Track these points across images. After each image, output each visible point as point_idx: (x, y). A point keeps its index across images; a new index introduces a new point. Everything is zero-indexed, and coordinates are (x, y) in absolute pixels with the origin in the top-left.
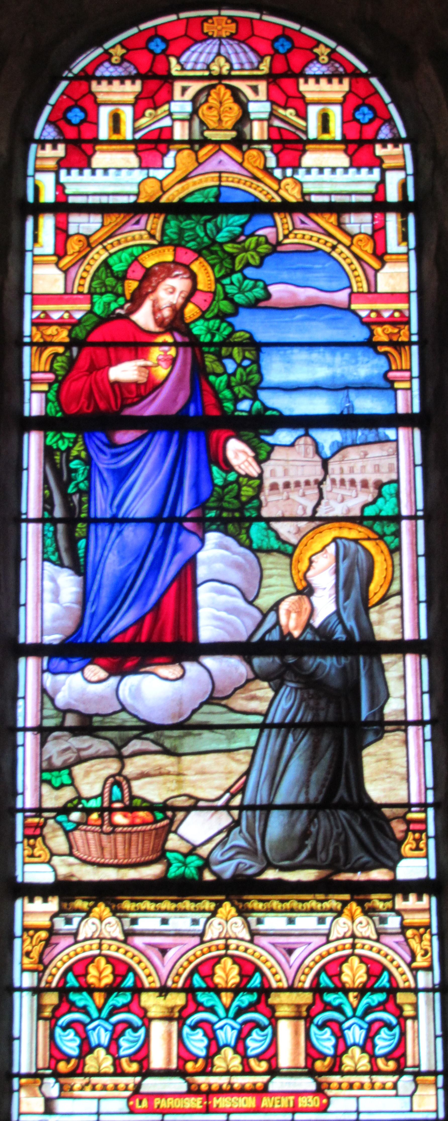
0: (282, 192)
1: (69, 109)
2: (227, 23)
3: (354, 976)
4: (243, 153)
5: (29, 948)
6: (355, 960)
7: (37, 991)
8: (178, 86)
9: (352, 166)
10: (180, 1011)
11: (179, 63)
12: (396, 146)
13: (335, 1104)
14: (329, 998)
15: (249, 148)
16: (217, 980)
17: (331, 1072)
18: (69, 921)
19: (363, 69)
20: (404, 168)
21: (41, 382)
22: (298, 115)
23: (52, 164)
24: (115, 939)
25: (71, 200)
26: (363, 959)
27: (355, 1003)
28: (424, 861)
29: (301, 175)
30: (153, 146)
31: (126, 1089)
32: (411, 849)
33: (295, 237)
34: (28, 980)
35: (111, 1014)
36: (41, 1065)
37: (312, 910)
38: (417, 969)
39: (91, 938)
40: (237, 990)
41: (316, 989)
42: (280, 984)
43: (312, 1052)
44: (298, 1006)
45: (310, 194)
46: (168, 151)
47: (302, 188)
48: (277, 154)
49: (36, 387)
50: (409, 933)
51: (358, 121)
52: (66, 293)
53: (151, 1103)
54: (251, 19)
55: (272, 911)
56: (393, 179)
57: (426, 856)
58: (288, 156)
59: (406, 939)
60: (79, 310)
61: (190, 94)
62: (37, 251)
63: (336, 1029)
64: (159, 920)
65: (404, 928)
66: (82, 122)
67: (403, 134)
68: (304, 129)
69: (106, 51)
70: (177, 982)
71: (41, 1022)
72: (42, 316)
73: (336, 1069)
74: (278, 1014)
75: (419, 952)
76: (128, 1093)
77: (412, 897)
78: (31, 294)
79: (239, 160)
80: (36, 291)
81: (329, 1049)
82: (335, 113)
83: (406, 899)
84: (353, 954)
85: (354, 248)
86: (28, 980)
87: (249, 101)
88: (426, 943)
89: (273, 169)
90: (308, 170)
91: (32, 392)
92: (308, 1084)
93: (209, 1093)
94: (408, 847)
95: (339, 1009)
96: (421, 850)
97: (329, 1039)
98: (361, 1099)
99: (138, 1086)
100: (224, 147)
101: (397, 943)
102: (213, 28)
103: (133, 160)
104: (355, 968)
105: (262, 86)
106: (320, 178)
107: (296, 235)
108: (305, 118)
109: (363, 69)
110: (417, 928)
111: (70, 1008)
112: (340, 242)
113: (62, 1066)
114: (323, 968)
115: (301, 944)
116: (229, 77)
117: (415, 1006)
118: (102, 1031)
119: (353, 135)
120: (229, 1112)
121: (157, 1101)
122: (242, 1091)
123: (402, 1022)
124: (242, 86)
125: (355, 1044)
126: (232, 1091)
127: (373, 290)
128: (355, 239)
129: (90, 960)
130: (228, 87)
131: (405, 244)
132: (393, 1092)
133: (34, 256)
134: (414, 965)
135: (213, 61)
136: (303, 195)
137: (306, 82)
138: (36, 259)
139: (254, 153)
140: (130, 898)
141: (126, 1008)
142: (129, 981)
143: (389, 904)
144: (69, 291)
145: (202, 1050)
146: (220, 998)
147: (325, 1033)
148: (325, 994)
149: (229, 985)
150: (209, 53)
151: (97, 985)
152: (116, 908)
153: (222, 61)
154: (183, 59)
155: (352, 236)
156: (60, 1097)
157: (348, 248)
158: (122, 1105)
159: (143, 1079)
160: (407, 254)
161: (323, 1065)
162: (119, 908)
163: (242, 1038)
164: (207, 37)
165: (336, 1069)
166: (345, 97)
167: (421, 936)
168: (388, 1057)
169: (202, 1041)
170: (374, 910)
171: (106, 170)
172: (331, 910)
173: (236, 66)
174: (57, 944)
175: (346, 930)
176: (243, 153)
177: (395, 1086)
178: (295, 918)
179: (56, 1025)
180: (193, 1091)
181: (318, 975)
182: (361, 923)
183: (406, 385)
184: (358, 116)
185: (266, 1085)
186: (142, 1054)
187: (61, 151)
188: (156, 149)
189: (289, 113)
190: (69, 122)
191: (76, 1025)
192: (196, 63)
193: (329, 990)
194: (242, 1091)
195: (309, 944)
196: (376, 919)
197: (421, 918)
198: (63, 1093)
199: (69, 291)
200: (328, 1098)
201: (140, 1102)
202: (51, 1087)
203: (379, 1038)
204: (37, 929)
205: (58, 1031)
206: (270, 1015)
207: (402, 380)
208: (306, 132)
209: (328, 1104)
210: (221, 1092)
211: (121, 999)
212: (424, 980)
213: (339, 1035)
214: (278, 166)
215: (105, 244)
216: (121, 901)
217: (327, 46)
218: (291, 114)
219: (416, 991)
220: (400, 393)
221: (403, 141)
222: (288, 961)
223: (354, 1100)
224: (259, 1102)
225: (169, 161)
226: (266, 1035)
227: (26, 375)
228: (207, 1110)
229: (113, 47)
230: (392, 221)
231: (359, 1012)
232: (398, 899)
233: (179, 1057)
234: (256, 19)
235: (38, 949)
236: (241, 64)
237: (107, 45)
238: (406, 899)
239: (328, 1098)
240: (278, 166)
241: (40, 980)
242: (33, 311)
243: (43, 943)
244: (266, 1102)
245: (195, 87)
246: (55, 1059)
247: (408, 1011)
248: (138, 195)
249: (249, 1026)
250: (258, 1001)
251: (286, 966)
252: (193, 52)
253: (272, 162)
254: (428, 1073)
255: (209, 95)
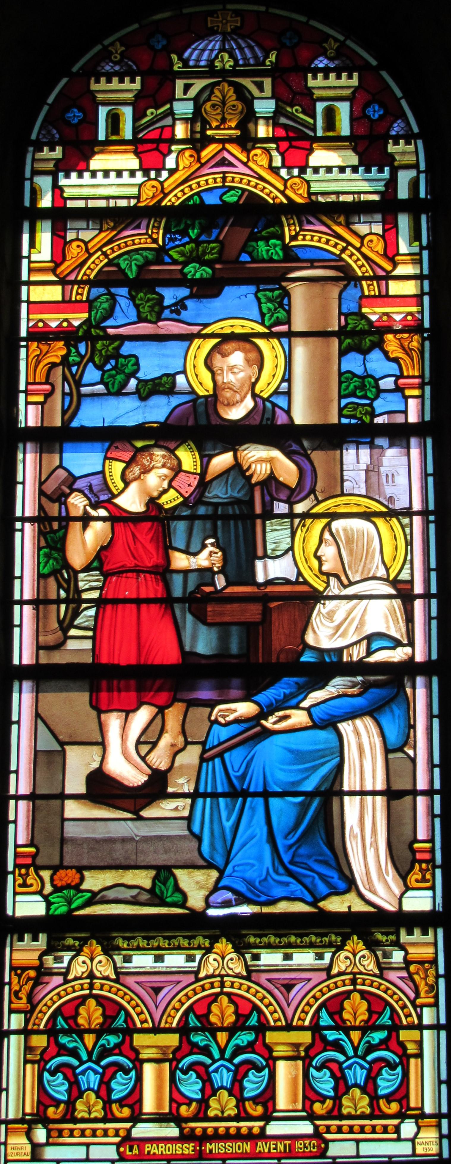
0: (289, 192)
1: (67, 110)
2: (231, 17)
3: (355, 1014)
4: (248, 152)
5: (17, 988)
6: (357, 996)
7: (26, 1032)
8: (180, 84)
9: (361, 164)
10: (174, 1052)
11: (180, 58)
12: (408, 143)
13: (334, 1150)
14: (64, 1040)
15: (254, 148)
16: (213, 1019)
17: (329, 1116)
18: (58, 960)
19: (374, 63)
20: (416, 166)
21: (36, 393)
22: (304, 112)
23: (50, 166)
24: (107, 978)
25: (70, 204)
26: (364, 995)
27: (223, 1044)
28: (430, 893)
29: (309, 175)
30: (154, 146)
31: (117, 1135)
32: (417, 881)
33: (304, 239)
34: (16, 1021)
35: (235, 1055)
36: (28, 1110)
37: (179, 948)
38: (422, 1006)
39: (212, 976)
40: (366, 1029)
41: (183, 1030)
42: (145, 1025)
43: (311, 1095)
44: (296, 1046)
45: (316, 194)
46: (170, 152)
47: (309, 187)
48: (282, 154)
49: (31, 399)
50: (412, 968)
51: (369, 117)
52: (63, 301)
53: (141, 1149)
54: (258, 13)
55: (138, 948)
56: (404, 178)
57: (433, 888)
58: (295, 156)
59: (410, 975)
60: (375, 313)
61: (193, 93)
62: (34, 258)
63: (70, 1074)
64: (183, 957)
65: (407, 962)
66: (81, 122)
67: (416, 130)
68: (312, 127)
69: (105, 48)
70: (304, 1020)
71: (29, 1066)
72: (65, 324)
73: (70, 1117)
74: (141, 1056)
75: (423, 988)
76: (117, 1140)
77: (417, 931)
78: (28, 302)
79: (245, 160)
80: (32, 299)
81: (328, 1091)
82: (343, 110)
83: (410, 933)
84: (222, 993)
85: (364, 250)
86: (16, 1021)
87: (253, 98)
88: (431, 980)
89: (278, 168)
90: (316, 170)
91: (27, 403)
92: (306, 1128)
93: (204, 1138)
94: (415, 877)
95: (206, 1051)
96: (427, 881)
97: (63, 1084)
98: (92, 1147)
99: (129, 1131)
100: (228, 146)
101: (401, 978)
102: (218, 22)
103: (132, 162)
104: (224, 1007)
105: (268, 83)
106: (119, 181)
107: (304, 236)
108: (314, 116)
109: (374, 63)
110: (421, 963)
111: (192, 1050)
112: (349, 244)
113: (317, 1107)
114: (190, 1009)
115: (302, 980)
116: (234, 72)
117: (420, 1044)
118: (225, 1071)
119: (362, 131)
120: (224, 1158)
121: (148, 1148)
122: (238, 1136)
123: (405, 1062)
124: (247, 82)
125: (222, 1087)
126: (227, 1137)
127: (384, 293)
128: (366, 240)
129: (213, 998)
130: (231, 84)
131: (417, 243)
132: (395, 1136)
133: (30, 262)
134: (419, 1001)
135: (217, 57)
136: (310, 194)
137: (315, 78)
138: (32, 265)
139: (258, 152)
140: (274, 932)
141: (250, 1047)
142: (253, 1021)
143: (393, 937)
144: (67, 298)
145: (197, 1093)
146: (215, 1038)
147: (58, 1077)
148: (193, 1034)
149: (225, 1025)
150: (212, 50)
151: (219, 1025)
152: (108, 945)
153: (226, 56)
154: (186, 55)
155: (362, 238)
156: (48, 1144)
157: (358, 250)
158: (111, 1153)
159: (402, 1122)
160: (420, 254)
161: (55, 1113)
162: (113, 945)
163: (372, 1078)
164: (212, 32)
165: (201, 1115)
166: (353, 93)
167: (426, 971)
168: (257, 1101)
169: (197, 1083)
170: (379, 943)
171: (106, 173)
172: (199, 948)
173: (241, 62)
174: (47, 983)
175: (84, 969)
176: (248, 152)
177: (397, 1129)
178: (292, 954)
179: (310, 1065)
180: (183, 1138)
181: (186, 1014)
182: (100, 962)
183: (416, 392)
184: (370, 111)
185: (263, 1129)
186: (267, 1095)
187: (58, 153)
188: (157, 149)
189: (296, 110)
190: (68, 123)
191: (196, 1068)
192: (198, 60)
193: (196, 1030)
194: (238, 1136)
195: (309, 980)
196: (248, 956)
197: (427, 952)
198: (51, 1140)
199: (67, 298)
200: (327, 1142)
201: (131, 1150)
202: (40, 1135)
203: (381, 1079)
204: (24, 969)
205: (312, 1071)
206: (267, 1056)
207: (412, 387)
208: (314, 130)
209: (327, 1148)
210: (216, 1137)
211: (244, 1038)
212: (428, 1016)
213: (205, 1078)
214: (284, 166)
215: (104, 249)
216: (245, 936)
217: (336, 40)
218: (297, 111)
219: (420, 1027)
220: (411, 401)
221: (416, 137)
222: (287, 1000)
223: (84, 1148)
224: (254, 1147)
225: (170, 162)
226: (131, 1078)
227: (22, 386)
228: (200, 1155)
229: (112, 44)
230: (404, 221)
231: (227, 1055)
232: (403, 932)
233: (172, 1100)
234: (262, 12)
235: (27, 987)
236: (245, 58)
237: (106, 42)
238: (410, 933)
239: (327, 1142)
240: (284, 166)
241: (27, 1021)
242: (28, 320)
243: (31, 982)
244: (262, 1147)
245: (199, 85)
246: (176, 1102)
247: (412, 1049)
248: (138, 197)
249: (113, 1069)
250: (123, 1042)
251: (284, 1004)
252: (195, 49)
253: (277, 161)
254: (431, 1116)
255: (212, 92)
